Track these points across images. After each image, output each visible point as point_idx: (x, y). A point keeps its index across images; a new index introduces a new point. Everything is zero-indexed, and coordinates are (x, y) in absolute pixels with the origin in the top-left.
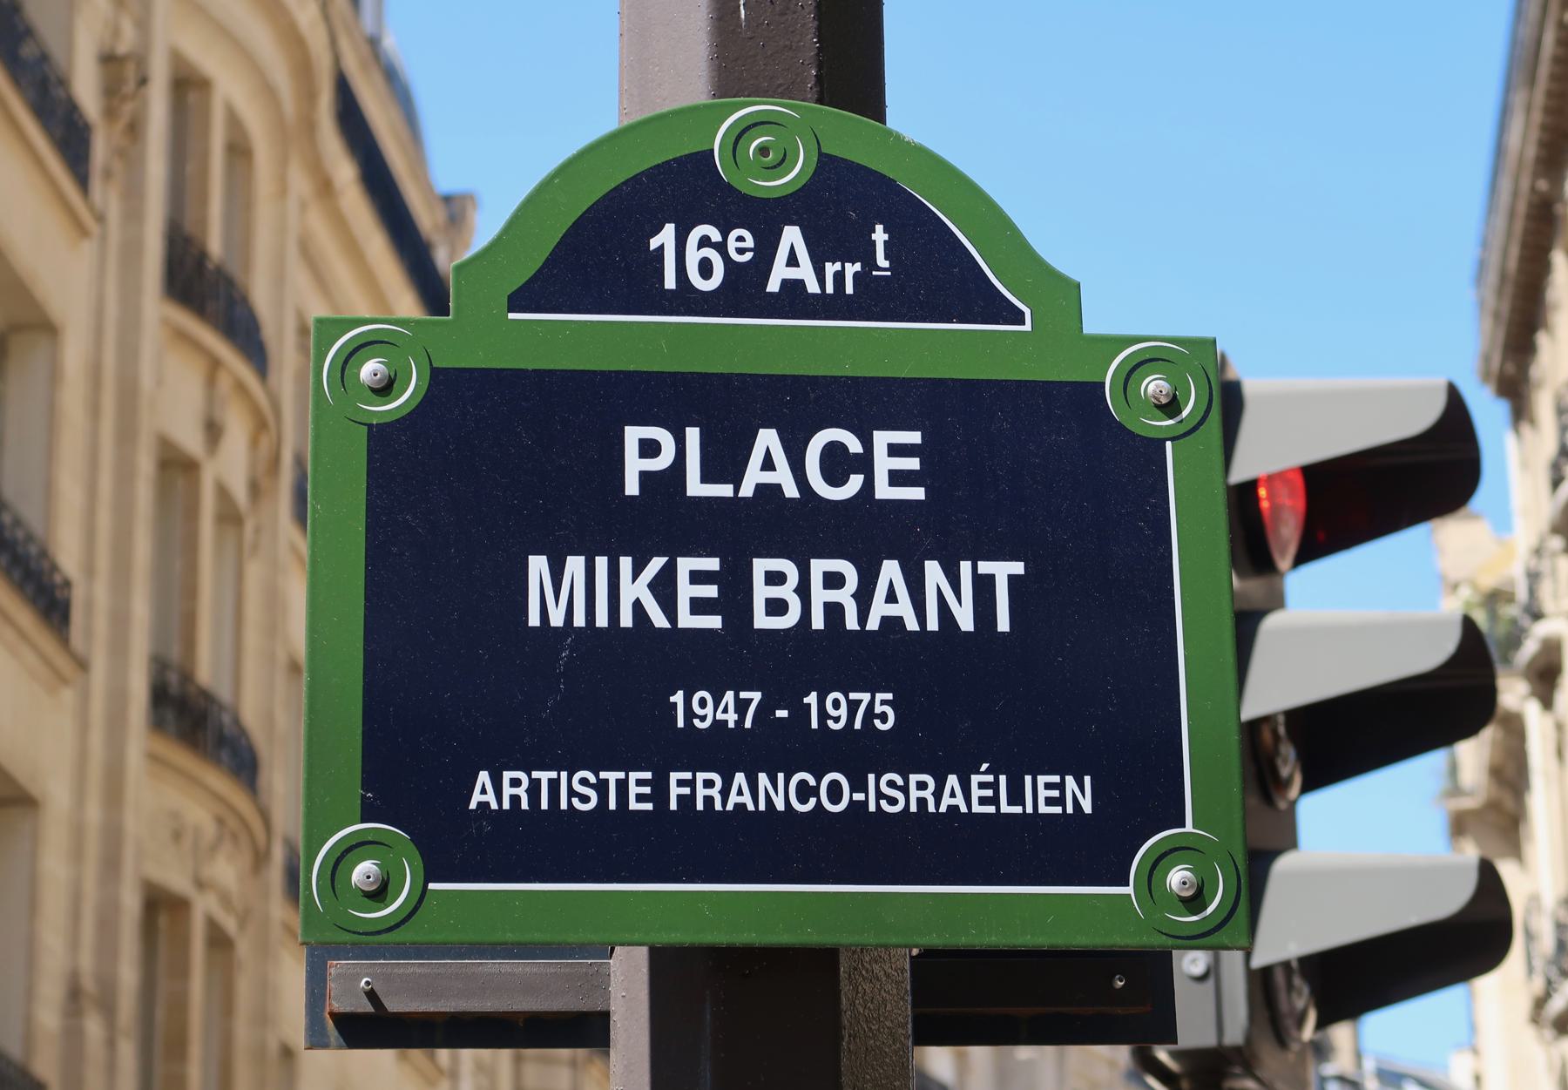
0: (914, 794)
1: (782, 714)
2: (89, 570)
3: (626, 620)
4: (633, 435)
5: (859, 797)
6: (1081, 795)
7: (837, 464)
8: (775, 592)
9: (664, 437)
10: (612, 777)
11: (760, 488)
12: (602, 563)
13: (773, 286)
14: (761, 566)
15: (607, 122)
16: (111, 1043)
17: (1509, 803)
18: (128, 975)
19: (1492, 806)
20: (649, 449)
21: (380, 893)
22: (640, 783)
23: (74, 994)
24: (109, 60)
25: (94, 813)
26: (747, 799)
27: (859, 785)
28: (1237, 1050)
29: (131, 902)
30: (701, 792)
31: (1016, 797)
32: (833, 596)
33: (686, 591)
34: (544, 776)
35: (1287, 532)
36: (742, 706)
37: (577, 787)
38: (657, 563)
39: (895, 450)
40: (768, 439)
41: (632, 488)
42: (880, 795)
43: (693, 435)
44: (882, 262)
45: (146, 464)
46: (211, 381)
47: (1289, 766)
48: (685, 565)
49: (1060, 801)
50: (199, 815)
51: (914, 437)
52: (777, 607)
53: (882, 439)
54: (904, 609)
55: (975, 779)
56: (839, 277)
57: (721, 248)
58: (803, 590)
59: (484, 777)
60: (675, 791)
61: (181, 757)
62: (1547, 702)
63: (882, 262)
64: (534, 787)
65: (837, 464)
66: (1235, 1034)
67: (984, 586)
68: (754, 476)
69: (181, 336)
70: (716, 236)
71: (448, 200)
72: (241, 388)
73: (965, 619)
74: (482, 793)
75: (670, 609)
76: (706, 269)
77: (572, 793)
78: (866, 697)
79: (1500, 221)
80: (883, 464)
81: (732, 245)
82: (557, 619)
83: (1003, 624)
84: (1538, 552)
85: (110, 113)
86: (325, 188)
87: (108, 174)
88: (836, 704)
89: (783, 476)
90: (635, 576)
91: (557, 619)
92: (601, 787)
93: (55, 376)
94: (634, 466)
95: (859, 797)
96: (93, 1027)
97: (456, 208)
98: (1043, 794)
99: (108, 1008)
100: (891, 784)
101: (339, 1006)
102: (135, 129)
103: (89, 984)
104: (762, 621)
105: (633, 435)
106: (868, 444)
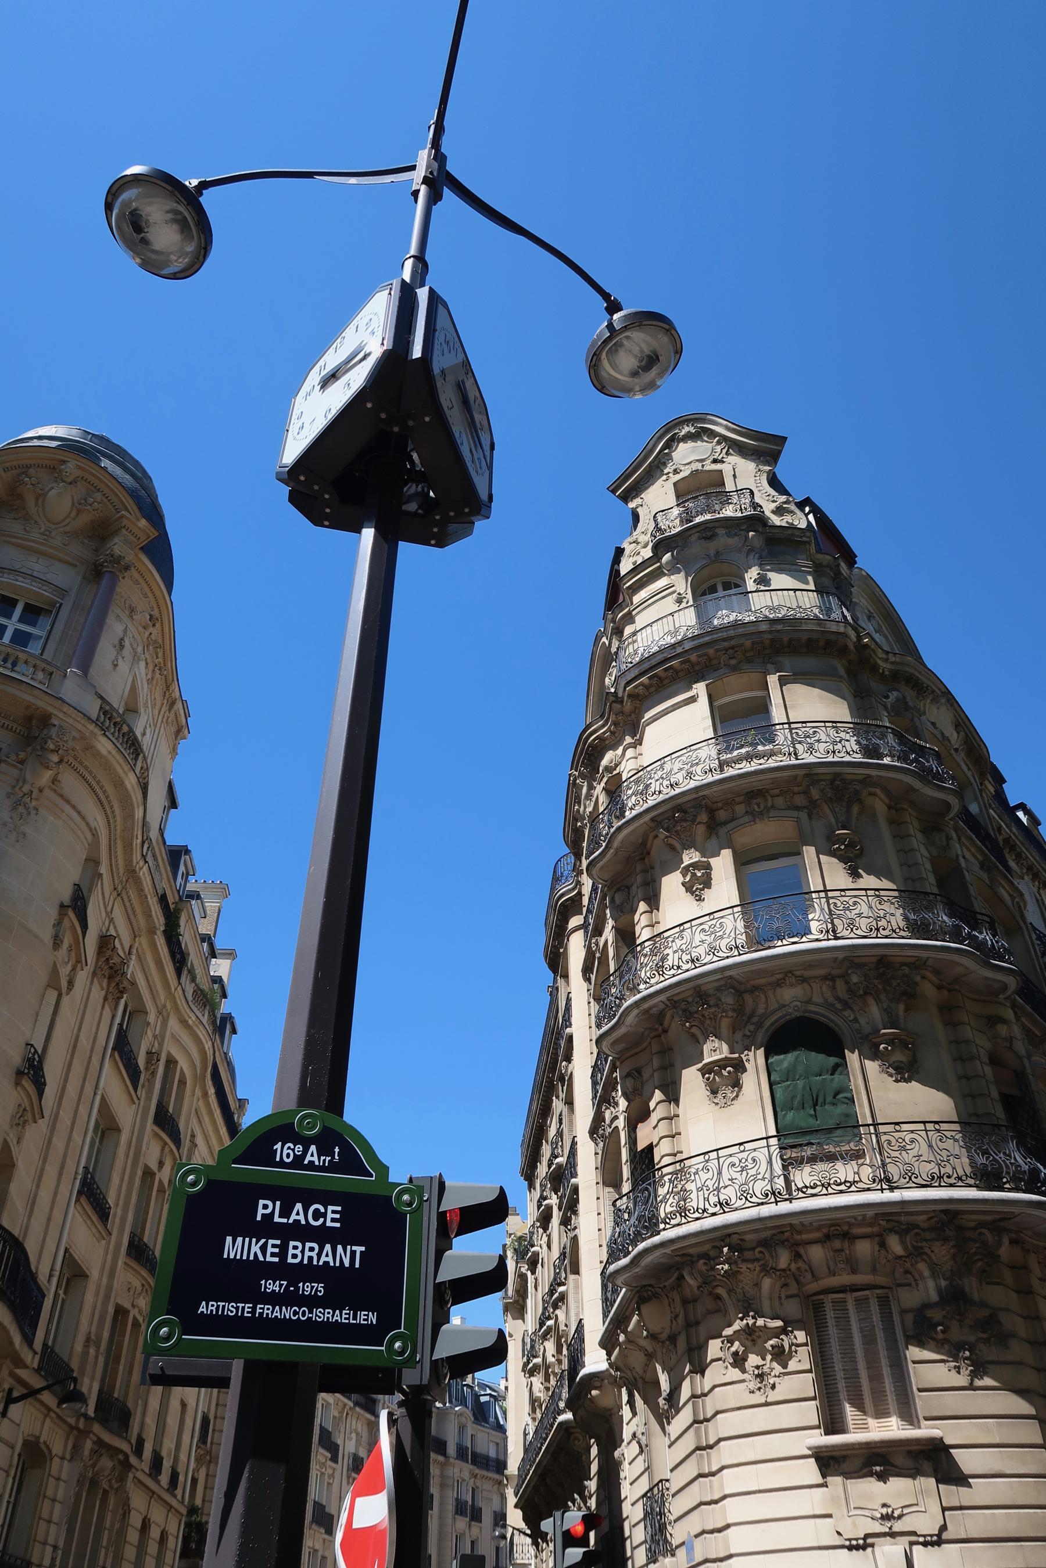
0: (326, 1315)
1: (292, 1289)
2: (117, 1205)
3: (252, 1258)
4: (261, 1202)
5: (310, 1315)
6: (373, 1318)
7: (317, 1215)
8: (295, 1252)
9: (269, 1203)
10: (241, 1305)
11: (295, 1220)
12: (247, 1240)
13: (306, 1162)
14: (292, 1243)
15: (269, 1112)
16: (97, 1357)
17: (521, 1302)
18: (106, 1335)
19: (516, 1302)
20: (265, 1207)
21: (168, 1338)
22: (249, 1308)
23: (88, 1340)
24: (149, 1053)
25: (105, 1280)
26: (330, 1259)
27: (311, 1312)
28: (425, 1385)
29: (111, 1310)
30: (266, 1311)
31: (355, 1318)
32: (311, 1254)
33: (270, 1250)
34: (221, 1304)
35: (454, 1226)
36: (281, 1286)
37: (231, 1308)
38: (263, 1241)
39: (333, 1212)
40: (299, 1206)
41: (259, 1218)
42: (316, 1315)
43: (278, 1203)
44: (337, 1157)
45: (139, 1173)
46: (163, 1150)
47: (448, 1297)
48: (271, 1242)
49: (367, 1320)
50: (137, 1283)
51: (339, 1208)
52: (295, 1256)
53: (330, 1208)
54: (278, 1314)
55: (344, 1312)
56: (324, 1161)
57: (293, 1150)
58: (303, 1252)
59: (204, 1303)
60: (258, 1311)
61: (134, 1264)
62: (533, 1273)
63: (337, 1157)
64: (218, 1307)
65: (317, 1215)
66: (425, 1381)
67: (353, 1253)
68: (293, 1217)
69: (156, 1135)
70: (292, 1147)
71: (240, 1100)
72: (171, 1151)
73: (347, 1264)
74: (202, 1309)
75: (264, 1255)
76: (288, 1156)
77: (228, 1310)
78: (316, 1285)
79: (529, 1130)
80: (330, 1216)
81: (296, 1149)
82: (232, 1257)
83: (357, 1266)
84: (533, 1226)
85: (147, 1069)
86: (206, 1095)
87: (143, 1086)
88: (308, 1287)
89: (301, 1218)
90: (256, 1244)
91: (232, 1257)
92: (237, 1308)
93: (117, 1145)
94: (261, 1211)
95: (310, 1315)
96: (92, 1351)
97: (242, 1103)
98: (363, 1317)
99: (98, 1346)
100: (320, 1312)
101: (151, 1372)
102: (153, 1074)
103: (93, 1337)
104: (290, 1260)
105: (261, 1202)
106: (326, 1210)
